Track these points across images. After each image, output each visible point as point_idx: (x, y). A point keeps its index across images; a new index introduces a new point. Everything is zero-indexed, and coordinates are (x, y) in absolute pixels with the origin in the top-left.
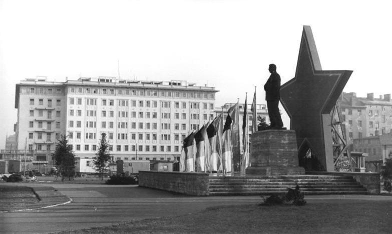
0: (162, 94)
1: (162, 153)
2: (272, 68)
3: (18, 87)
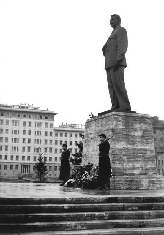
0: (7, 114)
1: (6, 161)
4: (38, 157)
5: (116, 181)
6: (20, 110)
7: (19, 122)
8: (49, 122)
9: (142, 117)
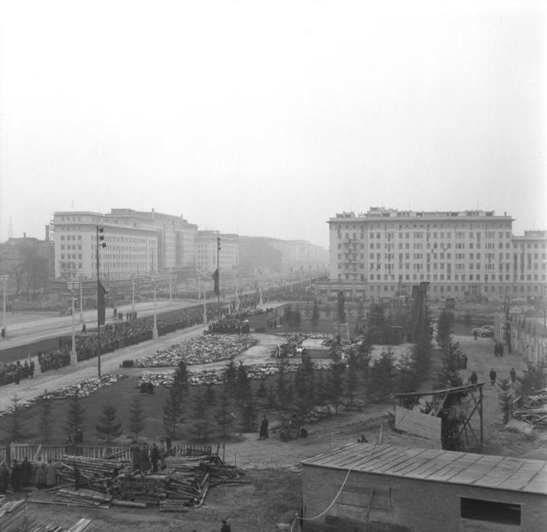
4: (418, 275)
5: (121, 300)
6: (469, 218)
7: (464, 234)
9: (98, 216)
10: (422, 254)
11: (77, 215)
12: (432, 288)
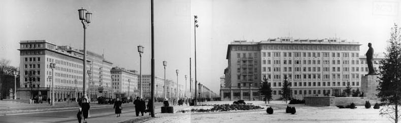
2: (370, 45)
3: (230, 47)
4: (346, 82)
8: (355, 52)
10: (300, 68)
11: (37, 43)
12: (293, 92)
